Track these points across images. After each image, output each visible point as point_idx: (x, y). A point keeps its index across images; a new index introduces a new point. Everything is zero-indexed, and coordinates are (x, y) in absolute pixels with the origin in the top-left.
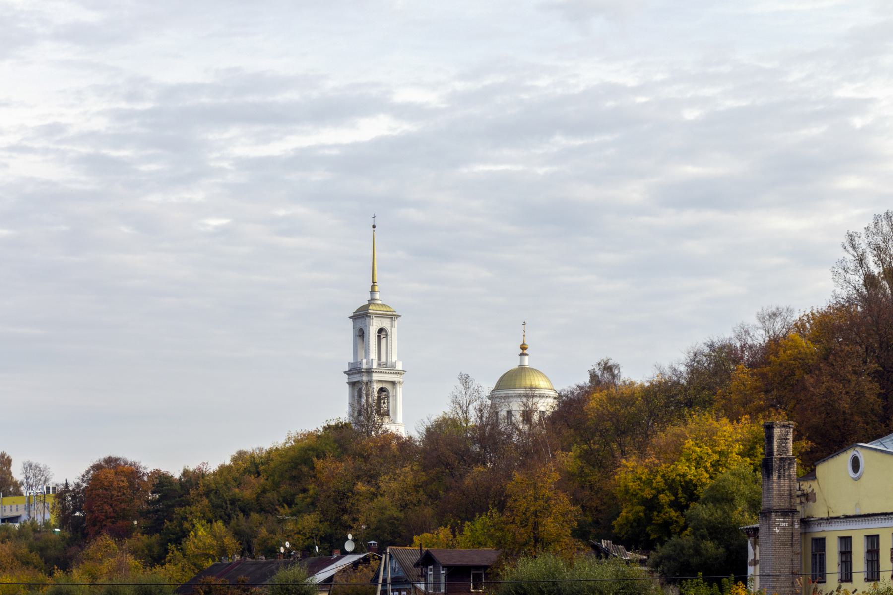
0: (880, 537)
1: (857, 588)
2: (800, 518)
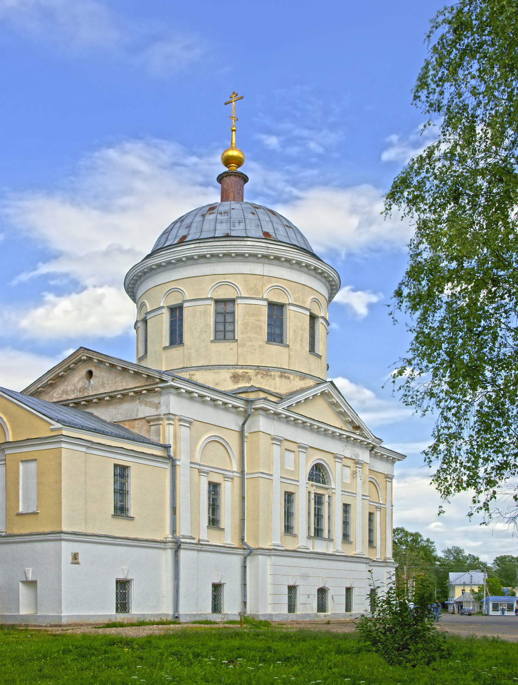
0: (298, 589)
1: (122, 576)
2: (318, 587)
